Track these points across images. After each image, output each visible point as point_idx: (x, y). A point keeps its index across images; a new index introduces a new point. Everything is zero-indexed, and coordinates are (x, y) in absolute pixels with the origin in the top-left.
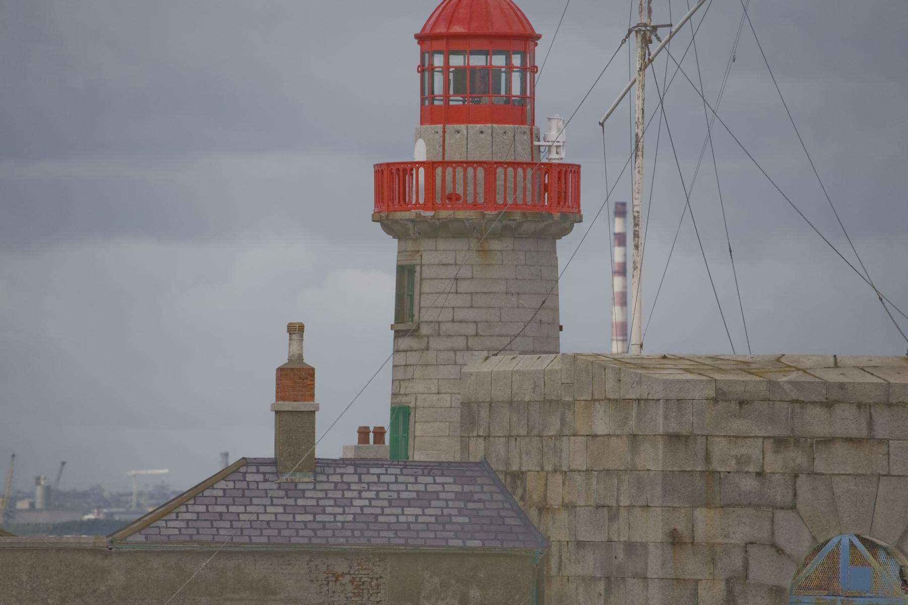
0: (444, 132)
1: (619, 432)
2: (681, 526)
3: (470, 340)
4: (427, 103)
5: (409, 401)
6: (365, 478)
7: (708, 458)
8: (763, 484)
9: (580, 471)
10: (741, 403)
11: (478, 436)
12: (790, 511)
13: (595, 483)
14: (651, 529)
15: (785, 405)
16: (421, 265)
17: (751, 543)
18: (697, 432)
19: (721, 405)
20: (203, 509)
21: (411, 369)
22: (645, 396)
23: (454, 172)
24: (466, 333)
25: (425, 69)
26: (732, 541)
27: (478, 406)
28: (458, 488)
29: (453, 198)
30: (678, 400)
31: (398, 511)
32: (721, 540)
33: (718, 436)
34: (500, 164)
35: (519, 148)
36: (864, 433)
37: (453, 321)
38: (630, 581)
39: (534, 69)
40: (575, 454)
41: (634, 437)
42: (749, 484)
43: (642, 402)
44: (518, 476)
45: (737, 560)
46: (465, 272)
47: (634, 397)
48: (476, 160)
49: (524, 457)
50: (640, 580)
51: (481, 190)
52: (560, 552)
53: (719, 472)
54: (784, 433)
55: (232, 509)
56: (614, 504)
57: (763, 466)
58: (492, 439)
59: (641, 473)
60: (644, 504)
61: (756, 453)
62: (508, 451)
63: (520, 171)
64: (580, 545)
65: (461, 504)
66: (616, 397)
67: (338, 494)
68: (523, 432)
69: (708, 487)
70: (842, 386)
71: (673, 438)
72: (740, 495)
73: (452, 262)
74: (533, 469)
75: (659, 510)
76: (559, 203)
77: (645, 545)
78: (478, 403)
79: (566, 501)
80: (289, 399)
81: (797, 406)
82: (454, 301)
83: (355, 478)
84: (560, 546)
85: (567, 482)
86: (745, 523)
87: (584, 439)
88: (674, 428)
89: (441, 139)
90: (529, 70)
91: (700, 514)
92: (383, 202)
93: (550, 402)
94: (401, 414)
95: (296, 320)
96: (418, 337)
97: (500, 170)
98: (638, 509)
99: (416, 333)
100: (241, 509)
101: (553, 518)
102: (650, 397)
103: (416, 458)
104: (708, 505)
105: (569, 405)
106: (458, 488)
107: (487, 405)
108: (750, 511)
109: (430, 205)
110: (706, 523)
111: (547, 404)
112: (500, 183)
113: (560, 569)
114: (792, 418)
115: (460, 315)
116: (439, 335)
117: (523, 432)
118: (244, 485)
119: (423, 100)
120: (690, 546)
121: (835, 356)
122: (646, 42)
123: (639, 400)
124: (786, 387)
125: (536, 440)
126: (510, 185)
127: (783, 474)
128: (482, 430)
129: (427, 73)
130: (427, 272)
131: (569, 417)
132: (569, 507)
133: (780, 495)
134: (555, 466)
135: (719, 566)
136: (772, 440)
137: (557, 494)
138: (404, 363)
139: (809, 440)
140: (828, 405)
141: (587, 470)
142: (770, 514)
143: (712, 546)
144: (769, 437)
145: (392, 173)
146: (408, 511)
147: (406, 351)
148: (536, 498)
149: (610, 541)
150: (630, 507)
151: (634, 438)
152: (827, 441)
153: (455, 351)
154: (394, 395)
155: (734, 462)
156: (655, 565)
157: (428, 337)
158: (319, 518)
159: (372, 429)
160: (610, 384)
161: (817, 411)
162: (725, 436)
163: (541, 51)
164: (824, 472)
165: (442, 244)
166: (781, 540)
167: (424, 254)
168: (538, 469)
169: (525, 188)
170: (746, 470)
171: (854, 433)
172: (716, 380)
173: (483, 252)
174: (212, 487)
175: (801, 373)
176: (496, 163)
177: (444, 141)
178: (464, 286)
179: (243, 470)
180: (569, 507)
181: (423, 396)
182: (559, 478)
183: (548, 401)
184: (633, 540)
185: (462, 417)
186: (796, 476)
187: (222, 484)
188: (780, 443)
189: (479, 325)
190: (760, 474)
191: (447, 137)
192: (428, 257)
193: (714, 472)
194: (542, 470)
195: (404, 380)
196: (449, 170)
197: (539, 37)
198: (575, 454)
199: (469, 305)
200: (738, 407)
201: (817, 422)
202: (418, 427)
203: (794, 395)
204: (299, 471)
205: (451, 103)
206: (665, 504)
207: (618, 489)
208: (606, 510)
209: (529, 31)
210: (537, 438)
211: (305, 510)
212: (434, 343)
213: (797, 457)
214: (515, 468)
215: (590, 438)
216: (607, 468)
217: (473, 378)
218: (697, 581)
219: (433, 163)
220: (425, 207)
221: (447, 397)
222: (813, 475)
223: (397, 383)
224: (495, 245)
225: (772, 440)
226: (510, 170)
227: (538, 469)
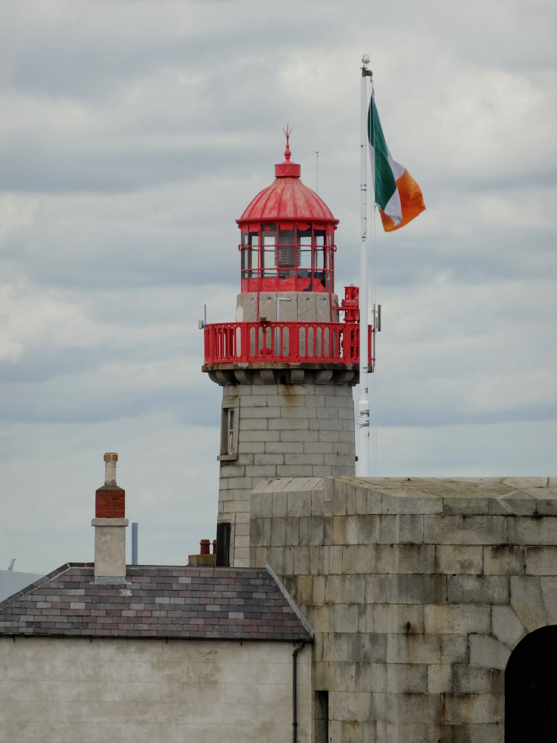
0: (258, 299)
1: (366, 542)
2: (414, 621)
3: (279, 468)
4: (246, 275)
7: (436, 563)
8: (483, 584)
9: (337, 575)
10: (464, 517)
11: (263, 546)
12: (506, 606)
13: (348, 584)
14: (389, 622)
15: (502, 518)
16: (240, 407)
17: (472, 633)
18: (427, 541)
19: (448, 519)
21: (232, 491)
22: (385, 512)
23: (273, 332)
24: (276, 463)
25: (246, 249)
26: (457, 632)
27: (263, 521)
30: (412, 515)
32: (447, 631)
33: (445, 545)
34: (302, 324)
35: (320, 312)
37: (265, 453)
38: (374, 665)
39: (333, 249)
40: (333, 562)
41: (377, 545)
42: (471, 584)
43: (383, 517)
45: (461, 649)
46: (275, 413)
47: (376, 512)
49: (296, 562)
50: (382, 665)
51: (286, 344)
52: (323, 642)
53: (446, 575)
54: (501, 542)
56: (362, 602)
57: (483, 571)
58: (273, 549)
59: (383, 576)
60: (385, 602)
61: (477, 559)
62: (284, 558)
63: (311, 329)
64: (338, 635)
68: (296, 543)
69: (435, 586)
71: (410, 547)
72: (463, 594)
73: (264, 404)
74: (303, 573)
75: (396, 606)
76: (352, 356)
77: (385, 636)
78: (263, 519)
79: (327, 600)
80: (104, 516)
81: (511, 519)
82: (265, 436)
84: (323, 637)
85: (328, 584)
86: (467, 617)
87: (340, 548)
88: (408, 538)
89: (256, 305)
90: (329, 250)
91: (431, 610)
92: (209, 356)
93: (315, 517)
94: (224, 529)
95: (111, 450)
96: (237, 466)
98: (380, 606)
99: (235, 463)
101: (318, 614)
102: (389, 513)
103: (236, 565)
104: (437, 602)
107: (269, 520)
108: (472, 607)
109: (245, 358)
110: (434, 617)
111: (313, 518)
112: (302, 340)
113: (322, 656)
114: (507, 529)
115: (271, 448)
116: (254, 464)
117: (296, 543)
119: (243, 273)
120: (421, 637)
121: (548, 478)
123: (381, 515)
124: (502, 504)
125: (305, 549)
126: (311, 341)
127: (500, 576)
128: (265, 541)
129: (246, 252)
130: (245, 413)
131: (329, 531)
132: (329, 604)
133: (497, 592)
134: (319, 571)
135: (446, 653)
136: (490, 548)
138: (227, 488)
139: (521, 548)
140: (537, 516)
141: (343, 574)
142: (489, 610)
143: (440, 637)
144: (487, 546)
145: (216, 333)
147: (228, 478)
148: (305, 597)
149: (359, 633)
150: (374, 604)
152: (536, 548)
154: (220, 514)
155: (458, 566)
157: (245, 466)
159: (211, 542)
160: (360, 503)
161: (529, 523)
162: (451, 545)
163: (340, 235)
164: (533, 573)
165: (256, 389)
166: (496, 631)
167: (242, 399)
168: (306, 573)
169: (315, 340)
170: (469, 572)
172: (443, 498)
173: (289, 396)
176: (299, 323)
177: (258, 306)
178: (274, 424)
180: (329, 604)
181: (241, 514)
182: (322, 580)
183: (314, 516)
184: (377, 632)
185: (251, 530)
188: (499, 549)
189: (286, 456)
190: (481, 576)
191: (261, 303)
192: (246, 401)
193: (441, 575)
194: (310, 574)
195: (227, 501)
197: (337, 222)
199: (278, 439)
200: (462, 520)
201: (528, 532)
202: (237, 539)
203: (509, 510)
205: (265, 275)
206: (400, 602)
207: (366, 590)
208: (356, 606)
209: (328, 217)
210: (306, 548)
212: (250, 471)
213: (510, 562)
214: (289, 572)
215: (345, 547)
216: (357, 572)
217: (259, 498)
218: (428, 665)
219: (248, 324)
220: (241, 359)
223: (222, 503)
224: (298, 390)
225: (490, 548)
226: (311, 329)
227: (306, 573)
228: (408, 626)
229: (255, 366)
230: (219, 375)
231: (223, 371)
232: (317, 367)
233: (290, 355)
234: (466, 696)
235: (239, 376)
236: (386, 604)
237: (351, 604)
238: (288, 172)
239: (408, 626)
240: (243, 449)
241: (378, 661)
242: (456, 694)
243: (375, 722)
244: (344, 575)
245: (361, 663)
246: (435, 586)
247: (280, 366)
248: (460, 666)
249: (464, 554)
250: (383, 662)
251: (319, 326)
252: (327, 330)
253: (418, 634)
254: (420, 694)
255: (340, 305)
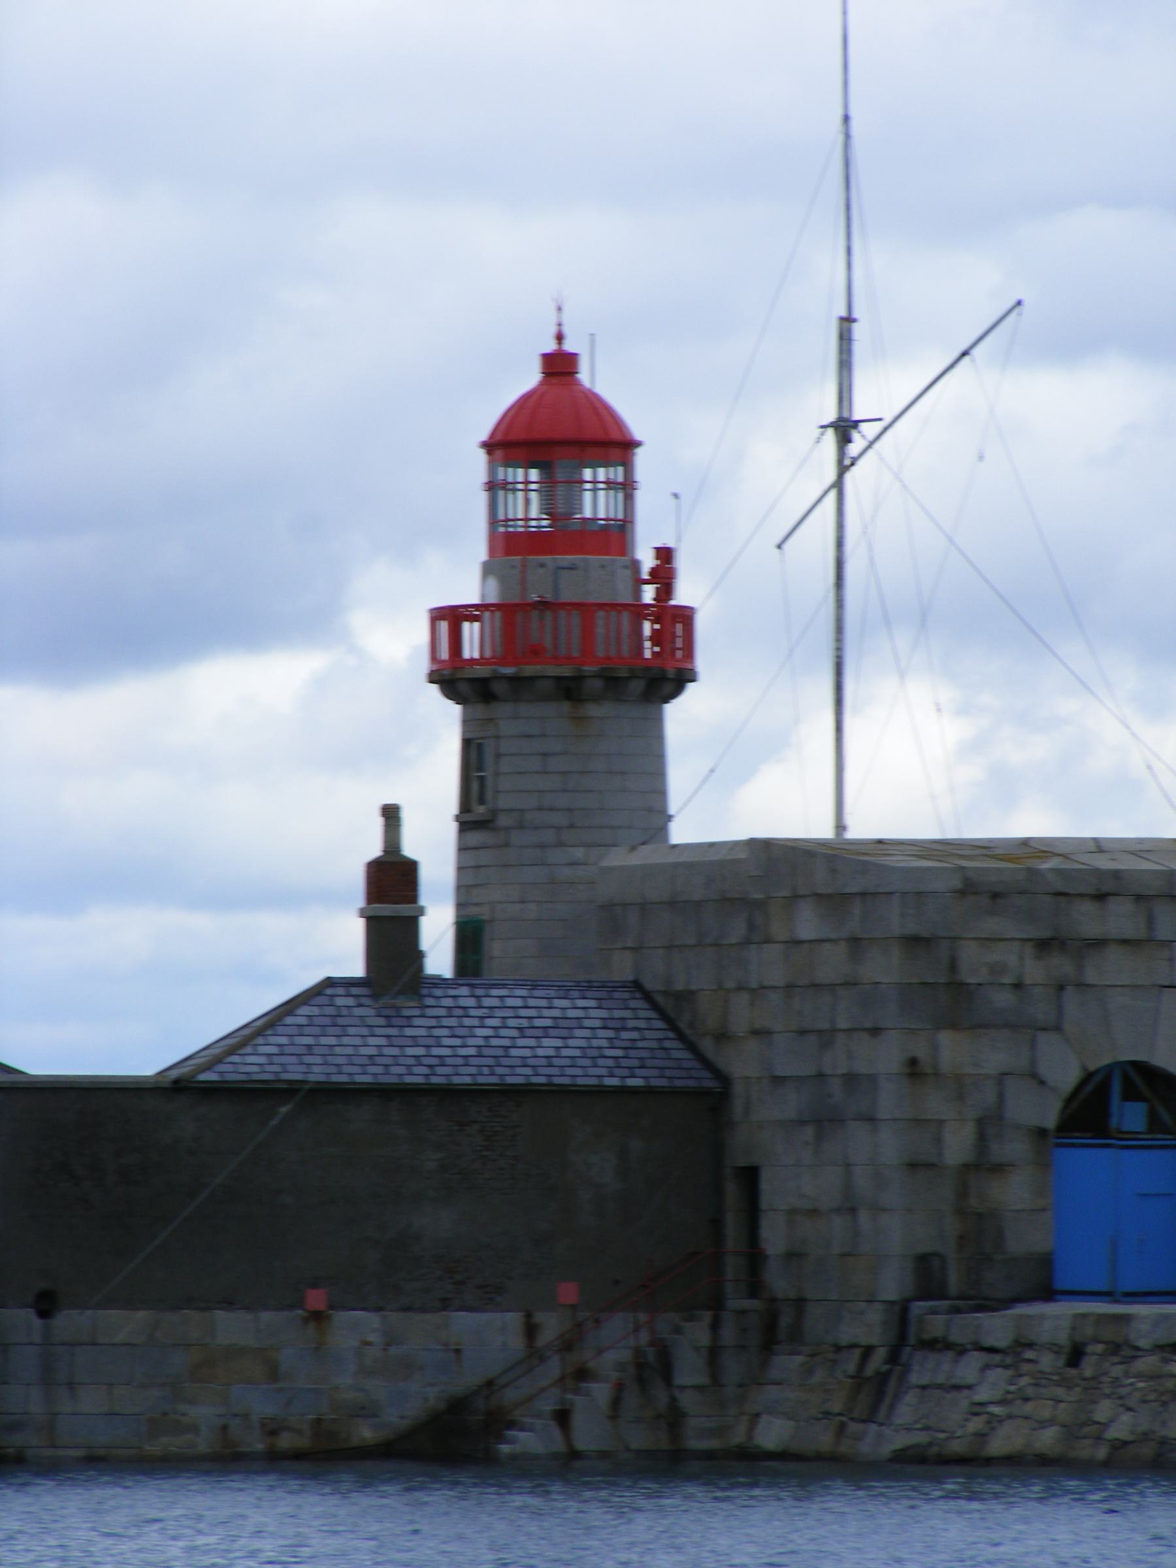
1: (833, 936)
2: (921, 1051)
5: (483, 913)
6: (487, 1002)
7: (953, 966)
14: (884, 1058)
20: (283, 1040)
28: (603, 1014)
29: (536, 652)
31: (532, 1042)
34: (601, 606)
36: (1143, 934)
40: (768, 965)
42: (1003, 999)
44: (686, 997)
48: (568, 601)
54: (1045, 934)
55: (324, 1041)
56: (824, 1025)
65: (610, 1034)
66: (830, 891)
67: (452, 1022)
69: (953, 1001)
70: (1117, 875)
71: (913, 942)
77: (873, 1078)
81: (1062, 899)
83: (471, 1002)
88: (912, 928)
90: (627, 487)
91: (945, 1038)
97: (601, 613)
100: (332, 1041)
104: (953, 1026)
105: (760, 905)
106: (603, 1014)
110: (952, 1050)
112: (600, 630)
118: (330, 1011)
122: (844, 439)
123: (863, 894)
137: (742, 1015)
146: (546, 1042)
151: (855, 942)
152: (1100, 943)
153: (542, 846)
156: (889, 1101)
158: (436, 1051)
161: (1088, 906)
163: (641, 458)
165: (524, 709)
166: (1043, 1070)
171: (1129, 934)
174: (290, 1013)
175: (1060, 859)
179: (329, 991)
182: (744, 997)
186: (1061, 988)
187: (304, 1010)
188: (1043, 945)
190: (1018, 986)
193: (962, 984)
196: (562, 614)
198: (768, 965)
201: (1087, 920)
203: (1059, 886)
204: (400, 993)
211: (415, 1041)
213: (1061, 965)
221: (532, 906)
222: (1081, 986)
224: (594, 710)
225: (1031, 943)
228: (913, 1062)
229: (529, 670)
230: (463, 688)
231: (471, 680)
232: (623, 673)
233: (567, 653)
234: (998, 1169)
235: (498, 688)
236: (875, 1031)
237: (802, 1032)
238: (559, 366)
239: (913, 1062)
240: (504, 802)
241: (860, 1118)
242: (983, 1165)
243: (853, 1210)
244: (790, 987)
245: (824, 1121)
246: (953, 1001)
247: (566, 671)
248: (989, 1125)
249: (995, 954)
250: (871, 1119)
251: (487, 610)
252: (498, 614)
253: (926, 1075)
254: (931, 1166)
255: (645, 576)
